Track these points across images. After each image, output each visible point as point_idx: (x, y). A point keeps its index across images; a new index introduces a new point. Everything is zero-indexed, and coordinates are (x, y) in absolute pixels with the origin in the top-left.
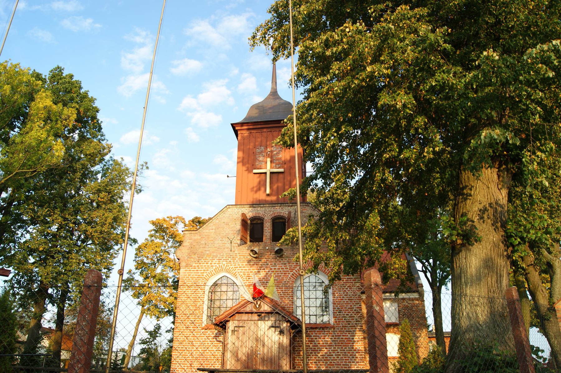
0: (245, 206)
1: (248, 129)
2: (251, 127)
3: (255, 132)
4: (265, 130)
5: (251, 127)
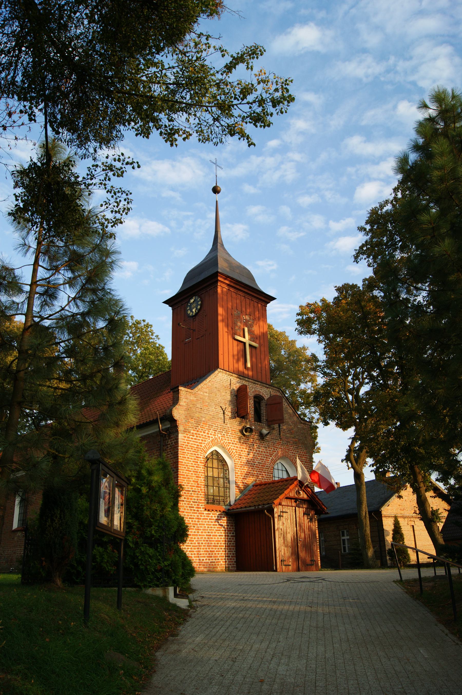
0: (233, 375)
1: (228, 285)
2: (232, 284)
3: (232, 290)
4: (241, 293)
5: (232, 284)
